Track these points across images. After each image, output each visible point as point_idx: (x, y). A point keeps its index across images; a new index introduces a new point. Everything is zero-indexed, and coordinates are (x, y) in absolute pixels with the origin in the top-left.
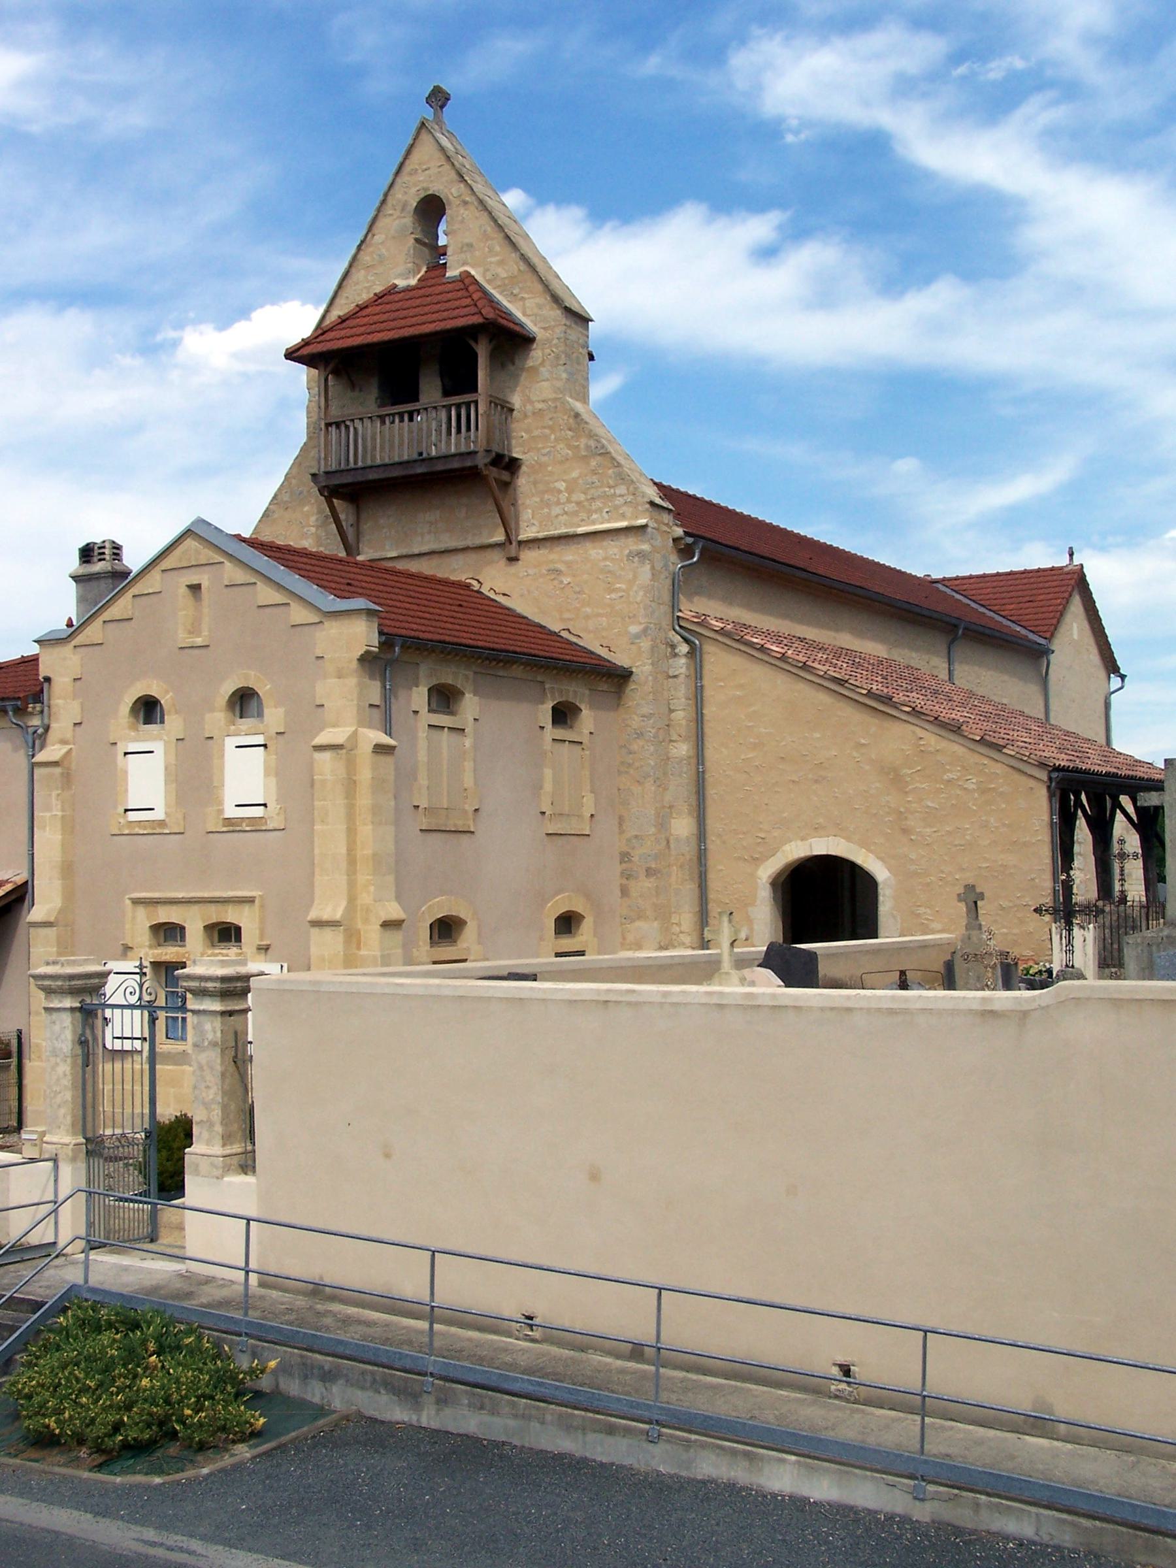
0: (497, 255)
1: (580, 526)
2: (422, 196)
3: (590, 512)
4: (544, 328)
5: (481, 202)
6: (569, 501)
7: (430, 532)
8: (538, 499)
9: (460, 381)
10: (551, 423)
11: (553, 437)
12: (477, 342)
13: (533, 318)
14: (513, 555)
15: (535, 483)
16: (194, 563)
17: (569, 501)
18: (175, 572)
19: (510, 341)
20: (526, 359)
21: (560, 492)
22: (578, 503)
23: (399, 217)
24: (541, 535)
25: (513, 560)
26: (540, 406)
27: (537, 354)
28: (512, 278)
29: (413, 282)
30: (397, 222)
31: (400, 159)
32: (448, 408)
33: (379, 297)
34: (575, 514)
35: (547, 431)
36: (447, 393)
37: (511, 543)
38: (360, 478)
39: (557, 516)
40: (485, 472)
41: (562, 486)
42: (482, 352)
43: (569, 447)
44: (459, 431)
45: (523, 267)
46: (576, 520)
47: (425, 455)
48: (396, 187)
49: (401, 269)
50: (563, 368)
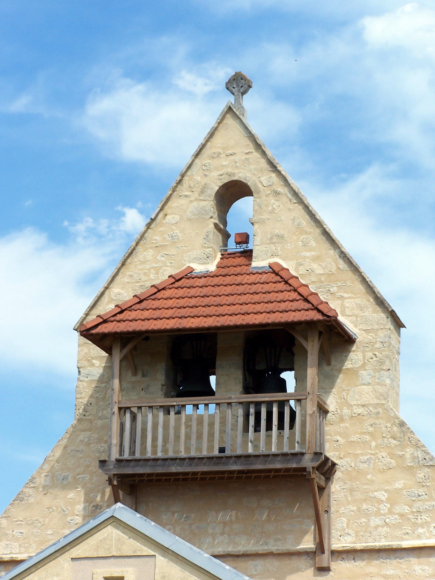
0: (311, 250)
1: (403, 539)
2: (226, 180)
3: (415, 525)
4: (365, 330)
5: (296, 194)
6: (390, 512)
7: (222, 534)
8: (355, 508)
9: (262, 377)
10: (371, 429)
11: (373, 444)
12: (306, 339)
13: (354, 318)
14: (325, 565)
15: (351, 490)
16: (115, 554)
17: (390, 512)
18: (90, 562)
19: (334, 338)
20: (343, 362)
21: (380, 501)
22: (402, 515)
23: (196, 200)
24: (359, 546)
25: (323, 570)
26: (360, 410)
27: (355, 357)
28: (330, 275)
29: (212, 267)
30: (195, 204)
31: (201, 140)
32: (246, 405)
33: (176, 280)
34: (398, 526)
35: (368, 438)
36: (247, 390)
37: (323, 552)
38: (160, 470)
39: (376, 527)
40: (313, 476)
41: (382, 495)
42: (312, 348)
43: (392, 455)
44: (281, 426)
45: (342, 264)
46: (398, 533)
47: (228, 453)
48: (194, 168)
49: (198, 252)
50: (386, 373)
